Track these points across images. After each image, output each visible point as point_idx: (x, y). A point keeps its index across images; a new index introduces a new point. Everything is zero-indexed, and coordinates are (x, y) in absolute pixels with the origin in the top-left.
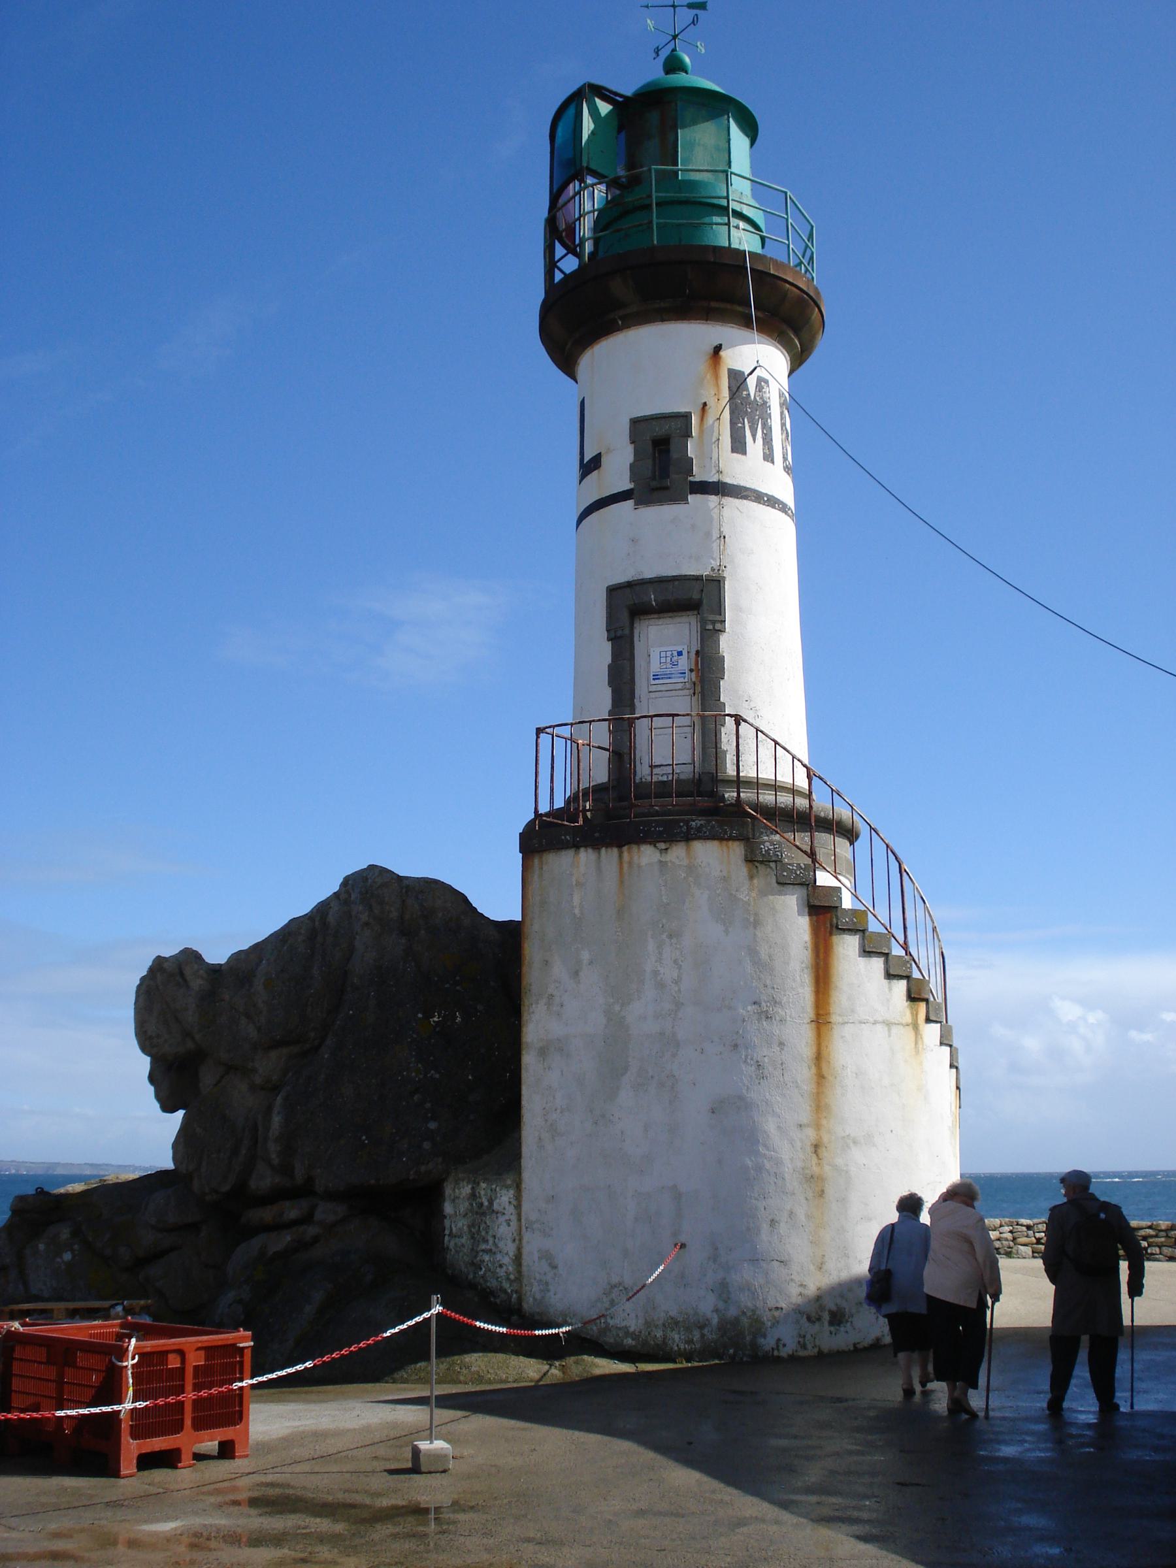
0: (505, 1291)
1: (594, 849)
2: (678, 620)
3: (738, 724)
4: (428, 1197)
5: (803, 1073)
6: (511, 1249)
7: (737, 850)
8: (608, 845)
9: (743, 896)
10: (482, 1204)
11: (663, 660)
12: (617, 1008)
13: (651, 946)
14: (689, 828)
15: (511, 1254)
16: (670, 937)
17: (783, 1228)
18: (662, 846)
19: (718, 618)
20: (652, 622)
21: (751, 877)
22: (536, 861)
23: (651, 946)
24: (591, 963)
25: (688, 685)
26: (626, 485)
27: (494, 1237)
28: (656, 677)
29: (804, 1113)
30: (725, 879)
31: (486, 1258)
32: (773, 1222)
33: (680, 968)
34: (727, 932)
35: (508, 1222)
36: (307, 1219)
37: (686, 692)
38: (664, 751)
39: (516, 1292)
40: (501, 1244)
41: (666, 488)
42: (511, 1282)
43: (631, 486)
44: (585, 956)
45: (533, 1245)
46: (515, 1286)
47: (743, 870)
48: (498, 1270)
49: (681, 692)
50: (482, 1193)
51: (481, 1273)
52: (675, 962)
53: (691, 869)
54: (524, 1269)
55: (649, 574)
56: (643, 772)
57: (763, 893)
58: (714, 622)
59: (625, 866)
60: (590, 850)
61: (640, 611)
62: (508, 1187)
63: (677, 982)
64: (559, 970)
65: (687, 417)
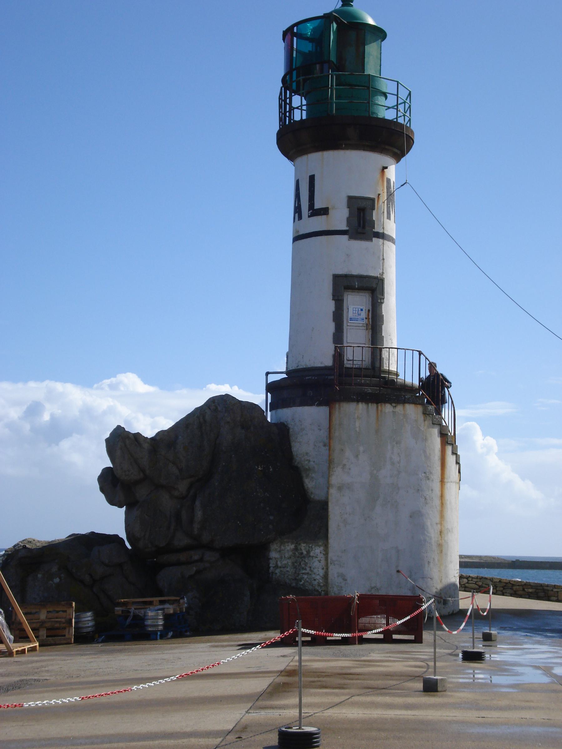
0: (317, 591)
1: (366, 403)
2: (361, 294)
3: (420, 355)
4: (264, 548)
5: (437, 502)
6: (322, 572)
7: (420, 409)
8: (372, 402)
9: (422, 429)
10: (302, 553)
11: (354, 312)
12: (375, 472)
13: (389, 447)
14: (405, 398)
15: (321, 575)
16: (397, 443)
17: (431, 565)
18: (394, 405)
19: (382, 297)
20: (350, 293)
21: (425, 421)
22: (337, 406)
23: (389, 447)
24: (364, 452)
25: (365, 325)
26: (344, 227)
27: (310, 567)
28: (351, 319)
29: (438, 520)
30: (416, 421)
31: (305, 576)
32: (429, 562)
33: (400, 457)
34: (416, 443)
35: (320, 561)
36: (201, 560)
37: (364, 328)
38: (356, 354)
39: (324, 591)
40: (315, 571)
41: (364, 233)
42: (321, 587)
43: (347, 228)
44: (361, 449)
45: (333, 571)
46: (323, 588)
47: (421, 417)
48: (313, 582)
49: (361, 328)
50: (303, 548)
51: (301, 583)
52: (398, 454)
53: (405, 415)
54: (329, 581)
55: (355, 272)
56: (347, 364)
57: (428, 427)
58: (381, 299)
59: (379, 412)
60: (364, 403)
61: (350, 288)
62: (319, 546)
63: (399, 463)
64: (348, 453)
65: (373, 200)
